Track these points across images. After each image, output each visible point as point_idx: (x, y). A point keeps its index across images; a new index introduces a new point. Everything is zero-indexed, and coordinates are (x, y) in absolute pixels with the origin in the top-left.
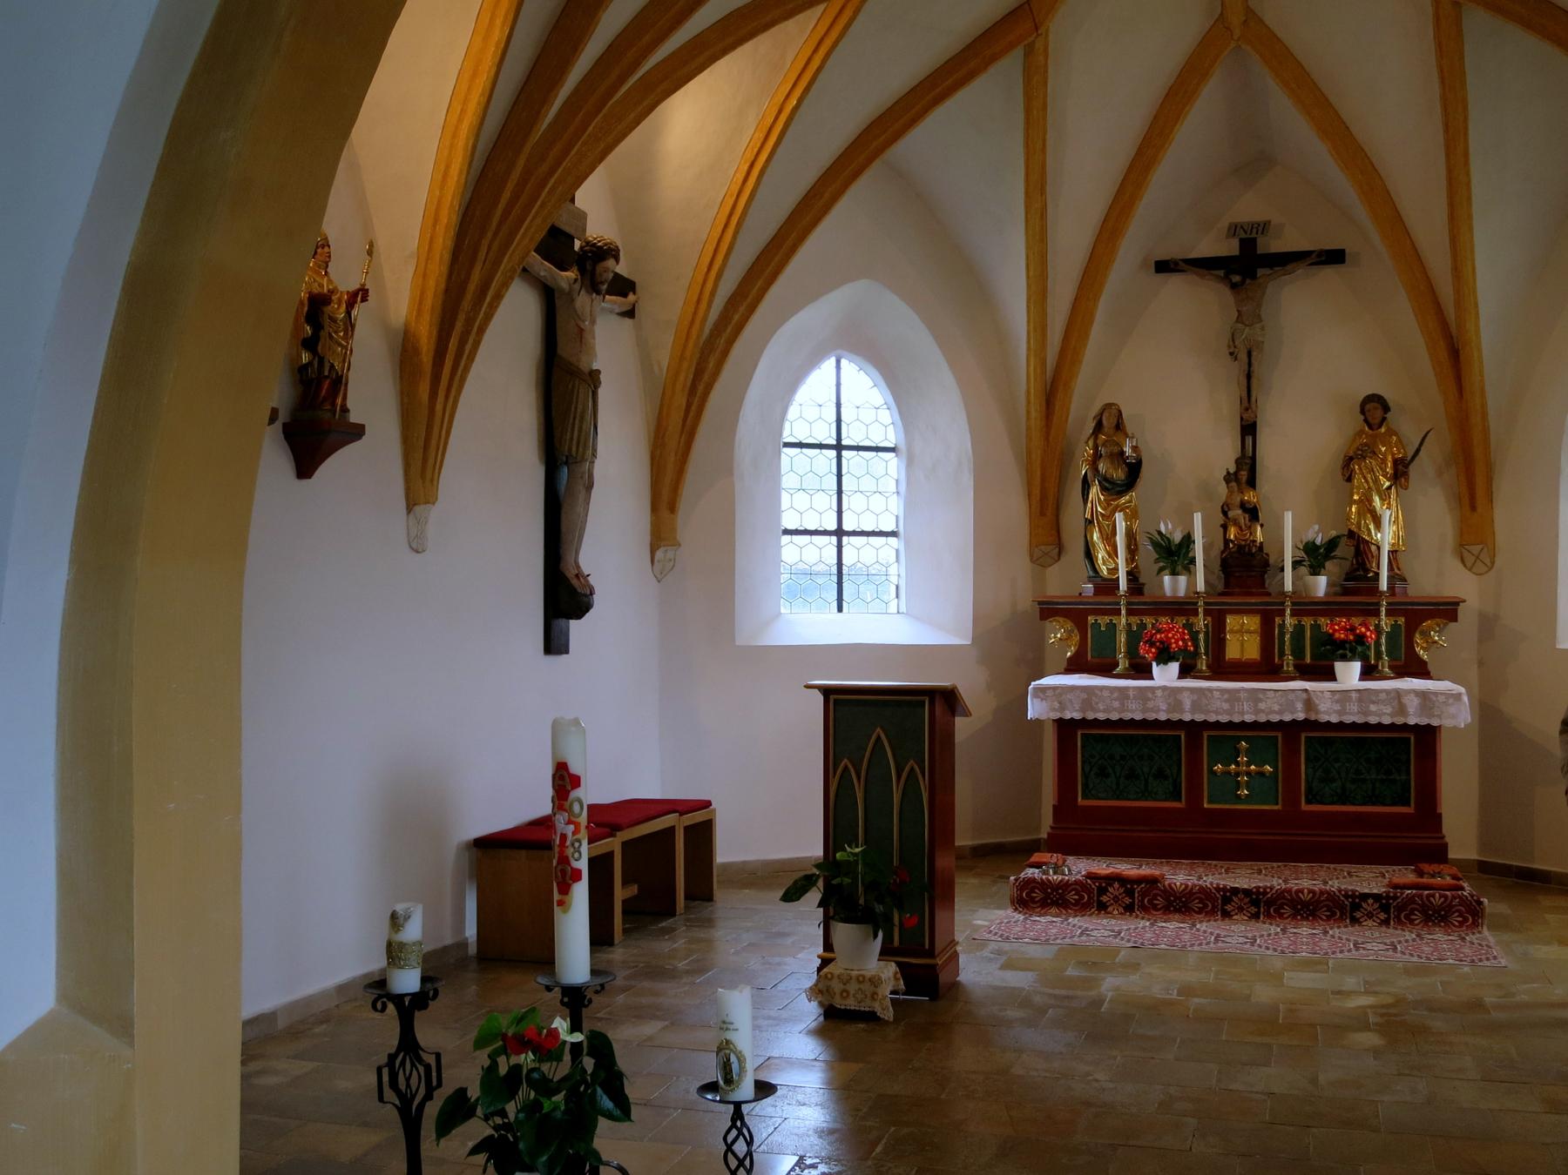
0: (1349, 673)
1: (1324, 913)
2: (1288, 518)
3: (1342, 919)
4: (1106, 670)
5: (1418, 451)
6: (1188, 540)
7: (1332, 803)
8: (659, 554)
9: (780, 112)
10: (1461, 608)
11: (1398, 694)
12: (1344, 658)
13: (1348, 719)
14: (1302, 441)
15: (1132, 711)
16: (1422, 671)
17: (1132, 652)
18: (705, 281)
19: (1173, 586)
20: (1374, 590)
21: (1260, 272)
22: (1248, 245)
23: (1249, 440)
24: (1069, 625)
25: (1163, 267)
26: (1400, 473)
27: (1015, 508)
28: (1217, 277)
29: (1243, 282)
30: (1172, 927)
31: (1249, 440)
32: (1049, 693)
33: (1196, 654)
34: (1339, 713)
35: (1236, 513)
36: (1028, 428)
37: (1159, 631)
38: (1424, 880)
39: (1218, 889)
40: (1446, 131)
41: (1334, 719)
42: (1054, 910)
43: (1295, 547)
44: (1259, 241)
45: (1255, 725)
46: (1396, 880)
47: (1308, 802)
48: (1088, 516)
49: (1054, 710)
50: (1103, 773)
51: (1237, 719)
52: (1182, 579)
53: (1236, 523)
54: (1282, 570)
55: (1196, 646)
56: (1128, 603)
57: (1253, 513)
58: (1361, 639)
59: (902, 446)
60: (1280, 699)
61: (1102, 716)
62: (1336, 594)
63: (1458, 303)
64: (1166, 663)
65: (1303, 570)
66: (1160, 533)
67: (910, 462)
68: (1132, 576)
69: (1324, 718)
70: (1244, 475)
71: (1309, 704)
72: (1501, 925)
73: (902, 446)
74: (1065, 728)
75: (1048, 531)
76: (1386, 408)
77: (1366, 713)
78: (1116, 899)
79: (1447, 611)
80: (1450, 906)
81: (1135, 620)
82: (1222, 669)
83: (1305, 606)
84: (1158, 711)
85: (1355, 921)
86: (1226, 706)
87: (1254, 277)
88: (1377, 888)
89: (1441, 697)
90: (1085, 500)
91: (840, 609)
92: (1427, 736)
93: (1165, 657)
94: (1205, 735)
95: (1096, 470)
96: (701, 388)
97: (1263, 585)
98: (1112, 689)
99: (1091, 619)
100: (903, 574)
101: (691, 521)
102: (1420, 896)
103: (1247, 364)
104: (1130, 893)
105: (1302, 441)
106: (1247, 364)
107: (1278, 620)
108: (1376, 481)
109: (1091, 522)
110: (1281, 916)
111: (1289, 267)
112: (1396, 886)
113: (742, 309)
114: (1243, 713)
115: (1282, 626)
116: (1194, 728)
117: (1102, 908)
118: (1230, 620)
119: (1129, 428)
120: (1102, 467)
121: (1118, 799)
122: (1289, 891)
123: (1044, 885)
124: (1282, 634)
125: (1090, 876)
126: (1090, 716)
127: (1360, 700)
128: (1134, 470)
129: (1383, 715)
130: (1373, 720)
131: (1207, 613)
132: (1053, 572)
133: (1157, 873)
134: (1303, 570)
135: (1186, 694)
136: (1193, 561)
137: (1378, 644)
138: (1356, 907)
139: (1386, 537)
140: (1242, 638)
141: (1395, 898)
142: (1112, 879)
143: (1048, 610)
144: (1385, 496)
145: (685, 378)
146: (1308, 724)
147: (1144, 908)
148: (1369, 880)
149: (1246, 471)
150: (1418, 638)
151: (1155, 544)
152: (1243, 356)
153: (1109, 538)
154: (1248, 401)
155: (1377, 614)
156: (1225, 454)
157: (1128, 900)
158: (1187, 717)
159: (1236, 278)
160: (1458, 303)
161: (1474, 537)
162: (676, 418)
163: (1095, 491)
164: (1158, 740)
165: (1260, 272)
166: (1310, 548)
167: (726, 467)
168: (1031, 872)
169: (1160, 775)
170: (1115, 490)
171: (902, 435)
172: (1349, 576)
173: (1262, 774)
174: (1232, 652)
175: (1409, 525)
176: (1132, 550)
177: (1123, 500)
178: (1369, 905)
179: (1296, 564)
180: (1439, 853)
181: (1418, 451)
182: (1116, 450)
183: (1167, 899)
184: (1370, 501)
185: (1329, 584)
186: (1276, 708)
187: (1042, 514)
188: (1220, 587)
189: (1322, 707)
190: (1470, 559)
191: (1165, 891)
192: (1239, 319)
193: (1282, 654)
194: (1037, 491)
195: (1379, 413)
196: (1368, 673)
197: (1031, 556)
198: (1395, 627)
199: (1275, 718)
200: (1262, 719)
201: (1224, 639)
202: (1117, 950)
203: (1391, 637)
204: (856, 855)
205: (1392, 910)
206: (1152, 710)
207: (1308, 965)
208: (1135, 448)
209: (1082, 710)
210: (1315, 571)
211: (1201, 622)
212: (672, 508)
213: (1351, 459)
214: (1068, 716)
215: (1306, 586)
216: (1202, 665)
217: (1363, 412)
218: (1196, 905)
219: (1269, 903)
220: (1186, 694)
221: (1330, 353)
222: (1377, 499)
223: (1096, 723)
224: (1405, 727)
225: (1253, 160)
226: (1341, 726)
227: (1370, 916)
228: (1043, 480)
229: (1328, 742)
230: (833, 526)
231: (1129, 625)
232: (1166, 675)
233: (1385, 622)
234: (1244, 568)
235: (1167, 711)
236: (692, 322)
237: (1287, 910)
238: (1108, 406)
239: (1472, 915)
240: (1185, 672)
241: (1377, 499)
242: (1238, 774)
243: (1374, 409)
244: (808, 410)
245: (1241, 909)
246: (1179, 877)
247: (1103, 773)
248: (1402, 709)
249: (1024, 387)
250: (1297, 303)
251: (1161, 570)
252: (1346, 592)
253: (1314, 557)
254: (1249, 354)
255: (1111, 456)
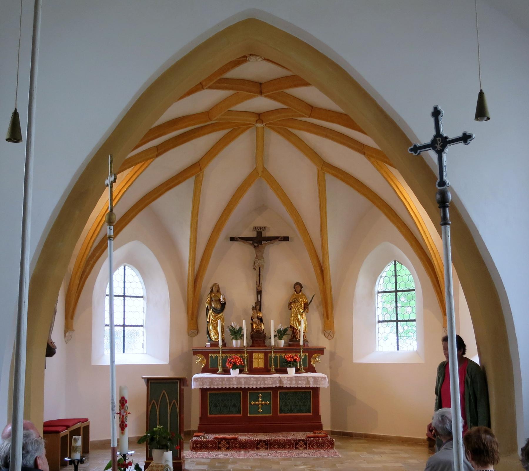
0: (291, 371)
1: (287, 446)
2: (272, 321)
3: (293, 448)
4: (215, 371)
5: (311, 301)
6: (241, 329)
7: (288, 413)
8: (67, 334)
9: (120, 192)
10: (325, 350)
11: (307, 378)
12: (290, 367)
13: (292, 386)
14: (275, 297)
15: (226, 385)
16: (313, 370)
17: (224, 365)
18: (89, 243)
19: (235, 344)
20: (299, 345)
21: (263, 242)
22: (259, 233)
23: (259, 296)
24: (203, 357)
25: (232, 239)
26: (306, 307)
27: (183, 318)
28: (250, 244)
29: (258, 246)
30: (242, 453)
31: (259, 296)
32: (199, 380)
33: (244, 366)
34: (289, 384)
35: (256, 320)
36: (188, 291)
37: (233, 359)
38: (317, 435)
39: (255, 440)
40: (320, 206)
41: (288, 386)
42: (204, 450)
43: (274, 331)
44: (263, 232)
45: (264, 389)
46: (308, 435)
47: (280, 413)
48: (208, 320)
49: (200, 385)
50: (216, 406)
51: (258, 387)
52: (239, 341)
53: (256, 323)
54: (271, 338)
55: (244, 363)
56: (222, 350)
57: (261, 320)
58: (295, 361)
59: (145, 296)
60: (272, 380)
61: (216, 387)
62: (286, 346)
63: (323, 255)
64: (235, 369)
65: (277, 338)
66: (232, 326)
67: (148, 302)
68: (223, 340)
69: (285, 386)
70: (258, 307)
71: (281, 381)
72: (339, 448)
73: (145, 296)
74: (204, 391)
75: (193, 324)
76: (302, 287)
77: (298, 384)
78: (224, 445)
79: (320, 351)
80: (324, 442)
81: (224, 355)
82: (252, 371)
83: (278, 350)
84: (234, 385)
85: (296, 448)
86: (255, 383)
87: (261, 243)
88: (303, 438)
89: (319, 378)
90: (207, 315)
91: (124, 352)
92: (316, 390)
93: (234, 367)
94: (248, 392)
95: (211, 305)
96: (84, 277)
97: (264, 343)
98: (219, 378)
99: (210, 355)
100: (145, 340)
101: (77, 323)
102: (316, 440)
103: (259, 272)
104: (228, 443)
105: (275, 297)
106: (259, 272)
107: (269, 355)
108: (299, 310)
109: (209, 322)
110: (274, 448)
111: (272, 242)
112: (308, 437)
113: (99, 252)
114: (260, 385)
115: (271, 356)
116: (245, 390)
117: (219, 448)
118: (255, 355)
119: (222, 291)
120: (213, 304)
121: (221, 414)
122: (277, 440)
123: (201, 442)
124: (271, 359)
125: (215, 438)
126: (212, 387)
127: (296, 380)
128: (223, 306)
129: (302, 384)
130: (300, 386)
131: (247, 352)
132: (195, 339)
133: (236, 436)
134: (277, 338)
135: (243, 379)
136: (243, 335)
137: (300, 362)
138: (297, 444)
139: (302, 328)
140: (258, 361)
141: (308, 440)
142: (222, 439)
143: (196, 352)
144: (301, 315)
145: (79, 274)
146: (280, 388)
147: (232, 448)
148: (300, 436)
149: (258, 306)
150: (312, 360)
151: (231, 330)
152: (258, 269)
153: (215, 328)
154: (259, 283)
155: (299, 352)
156: (251, 301)
157: (227, 446)
158: (243, 387)
159: (256, 245)
160: (323, 255)
161: (328, 328)
162: (75, 288)
163: (210, 312)
164: (233, 394)
165: (263, 242)
166: (279, 331)
167: (89, 303)
168: (196, 438)
169: (234, 406)
170: (217, 312)
171: (145, 293)
172: (291, 340)
173: (266, 404)
174: (255, 365)
175: (309, 324)
176: (223, 332)
177: (220, 315)
178: (301, 443)
179: (275, 336)
180: (320, 427)
181: (311, 301)
182: (217, 299)
183: (240, 445)
184: (297, 316)
185: (285, 343)
186: (271, 383)
187: (192, 319)
188: (251, 344)
189: (285, 382)
190: (327, 335)
191: (239, 442)
192: (256, 258)
193: (271, 365)
194: (190, 312)
195: (299, 288)
196: (297, 371)
197: (188, 333)
198: (305, 356)
199: (270, 386)
200: (266, 386)
201: (253, 361)
202: (228, 459)
203: (304, 360)
204: (160, 428)
205: (307, 444)
206: (232, 384)
207: (285, 460)
208: (224, 299)
209: (210, 385)
210: (280, 339)
211: (245, 356)
212: (72, 318)
213: (291, 303)
214: (205, 387)
215: (278, 344)
216: (246, 369)
217: (294, 288)
218: (249, 446)
219: (271, 444)
220: (243, 379)
221: (284, 269)
222: (299, 315)
223: (214, 389)
224: (309, 388)
225: (261, 207)
226: (290, 388)
227: (301, 446)
228: (193, 308)
229: (286, 394)
230: (126, 324)
231: (222, 357)
232: (234, 373)
233: (302, 355)
234: (258, 338)
235: (237, 385)
236: (83, 256)
237: (276, 446)
238: (215, 284)
239: (330, 445)
240: (241, 372)
241: (299, 315)
242: (258, 405)
243: (298, 287)
244: (385, 281)
245: (262, 447)
246: (243, 438)
247: (216, 406)
248: (308, 382)
249: (187, 277)
250: (274, 253)
251: (232, 339)
252: (290, 345)
253: (280, 334)
254: (260, 269)
255: (216, 301)
